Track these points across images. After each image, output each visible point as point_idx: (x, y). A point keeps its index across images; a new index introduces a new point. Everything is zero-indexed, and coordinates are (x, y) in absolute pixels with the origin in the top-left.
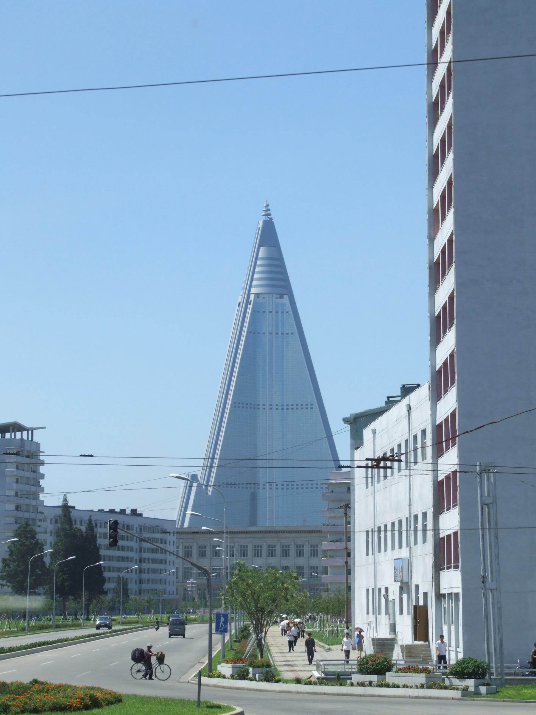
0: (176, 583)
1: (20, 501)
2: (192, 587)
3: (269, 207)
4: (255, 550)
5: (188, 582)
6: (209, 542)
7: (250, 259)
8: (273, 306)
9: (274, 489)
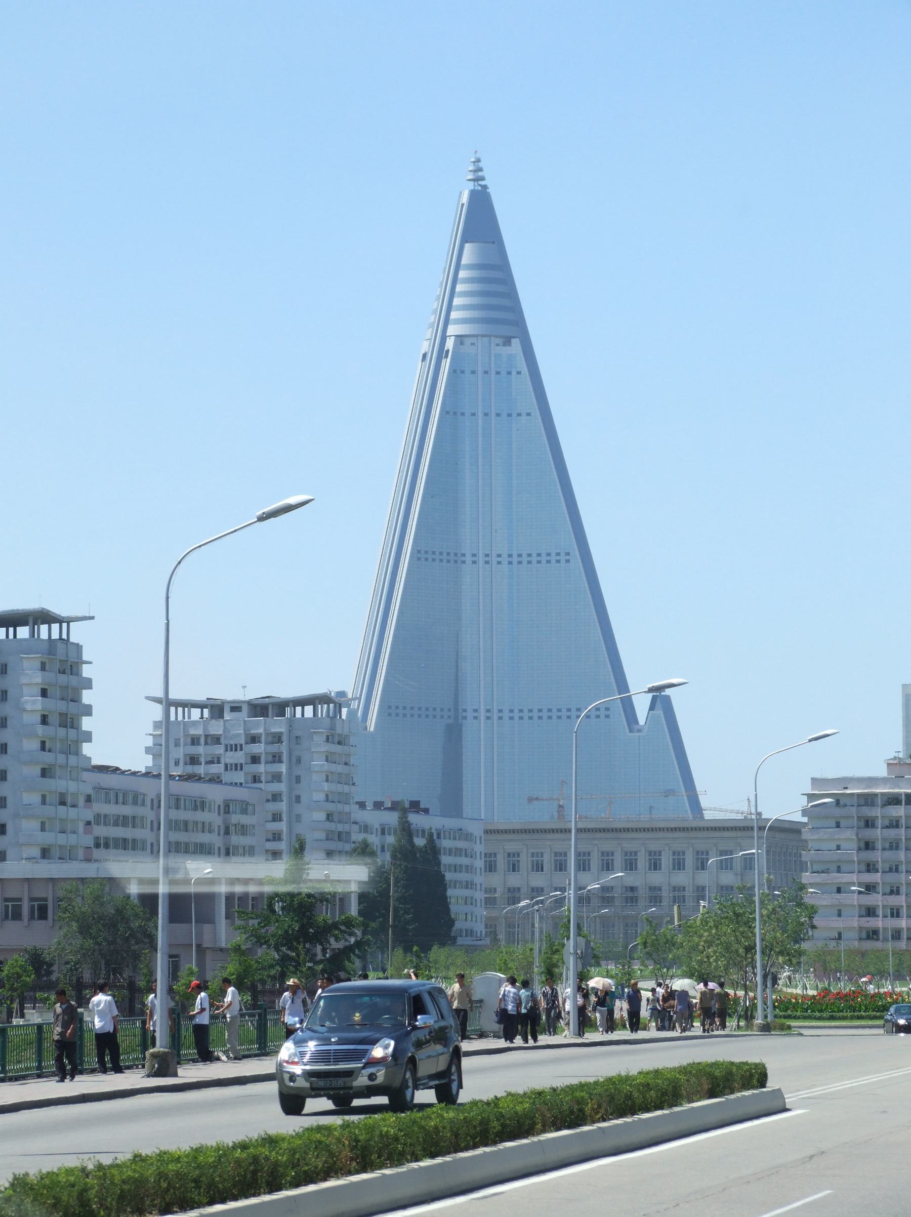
1: (331, 807)
3: (481, 164)
7: (445, 268)
9: (495, 717)
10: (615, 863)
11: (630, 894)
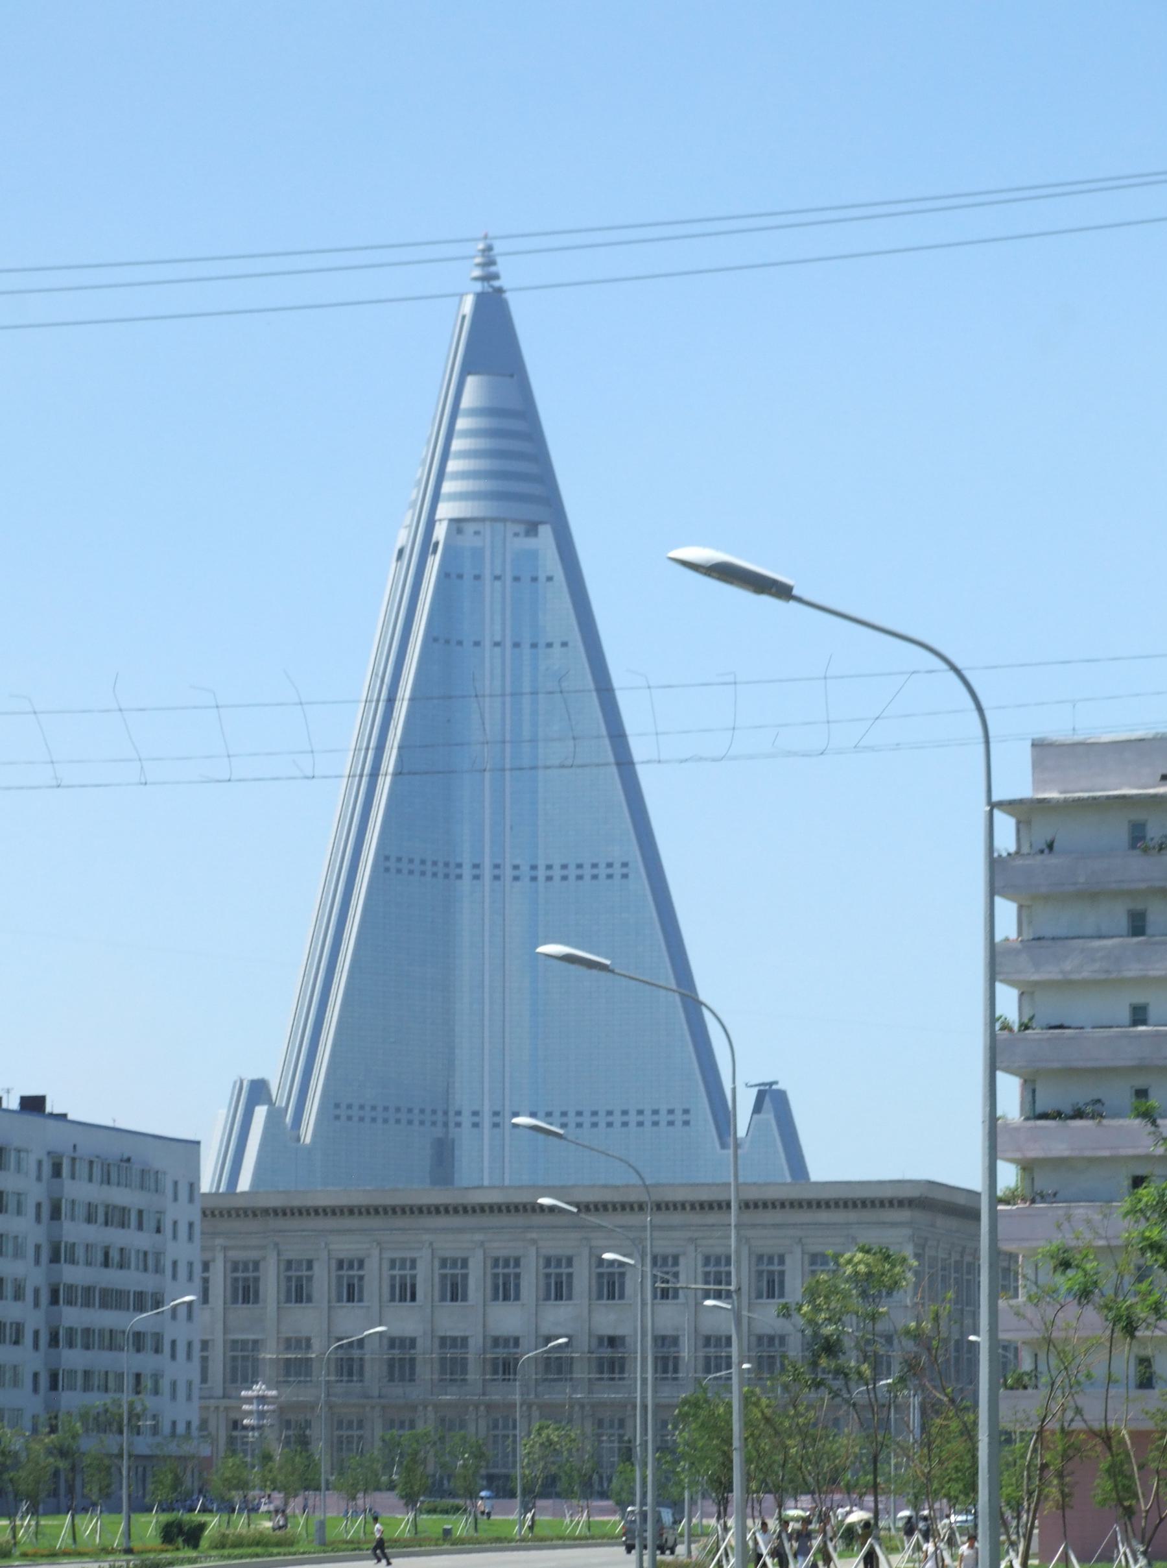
0: (201, 1398)
2: (261, 1415)
4: (496, 1276)
5: (243, 1393)
6: (323, 1245)
8: (504, 561)
10: (576, 1282)
11: (607, 1353)
